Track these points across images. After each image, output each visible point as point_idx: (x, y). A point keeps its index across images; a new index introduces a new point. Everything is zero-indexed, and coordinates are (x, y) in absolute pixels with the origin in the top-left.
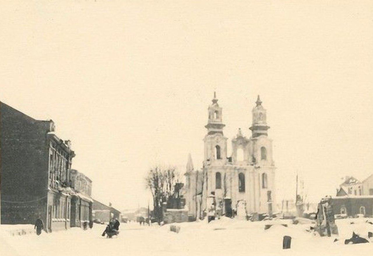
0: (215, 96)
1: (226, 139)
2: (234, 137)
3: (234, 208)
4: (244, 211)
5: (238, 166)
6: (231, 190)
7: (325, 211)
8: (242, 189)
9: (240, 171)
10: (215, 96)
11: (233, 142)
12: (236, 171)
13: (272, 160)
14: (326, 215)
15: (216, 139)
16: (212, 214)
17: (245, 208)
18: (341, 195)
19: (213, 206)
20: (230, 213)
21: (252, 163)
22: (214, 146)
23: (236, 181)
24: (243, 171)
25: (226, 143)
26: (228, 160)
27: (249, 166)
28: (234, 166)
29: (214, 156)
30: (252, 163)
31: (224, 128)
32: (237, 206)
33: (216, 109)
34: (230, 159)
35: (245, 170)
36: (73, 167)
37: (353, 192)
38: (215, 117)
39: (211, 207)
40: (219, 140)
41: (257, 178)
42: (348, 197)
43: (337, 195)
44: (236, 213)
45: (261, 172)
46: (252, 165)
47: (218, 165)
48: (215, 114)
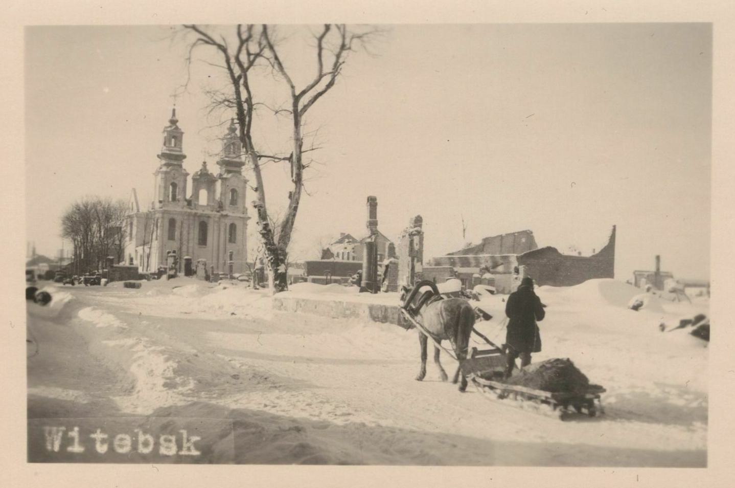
0: (174, 114)
1: (187, 174)
2: (197, 173)
3: (194, 268)
4: (204, 271)
5: (200, 212)
6: (188, 243)
7: (258, 275)
8: (203, 241)
9: (202, 219)
10: (174, 114)
11: (194, 180)
12: (196, 218)
13: (244, 207)
14: (258, 278)
15: (172, 174)
16: (172, 272)
17: (205, 269)
18: (324, 259)
19: (173, 265)
20: (190, 272)
21: (218, 209)
22: (169, 183)
23: (195, 233)
24: (205, 219)
25: (185, 181)
26: (186, 203)
27: (214, 213)
28: (194, 211)
29: (168, 196)
30: (218, 209)
31: (184, 160)
32: (197, 267)
33: (175, 134)
34: (189, 203)
35: (209, 217)
36: (358, 239)
37: (341, 256)
38: (173, 145)
39: (172, 266)
40: (176, 175)
41: (222, 229)
42: (335, 261)
43: (323, 258)
44: (195, 272)
45: (228, 222)
46: (218, 212)
47: (178, 208)
48: (173, 140)
